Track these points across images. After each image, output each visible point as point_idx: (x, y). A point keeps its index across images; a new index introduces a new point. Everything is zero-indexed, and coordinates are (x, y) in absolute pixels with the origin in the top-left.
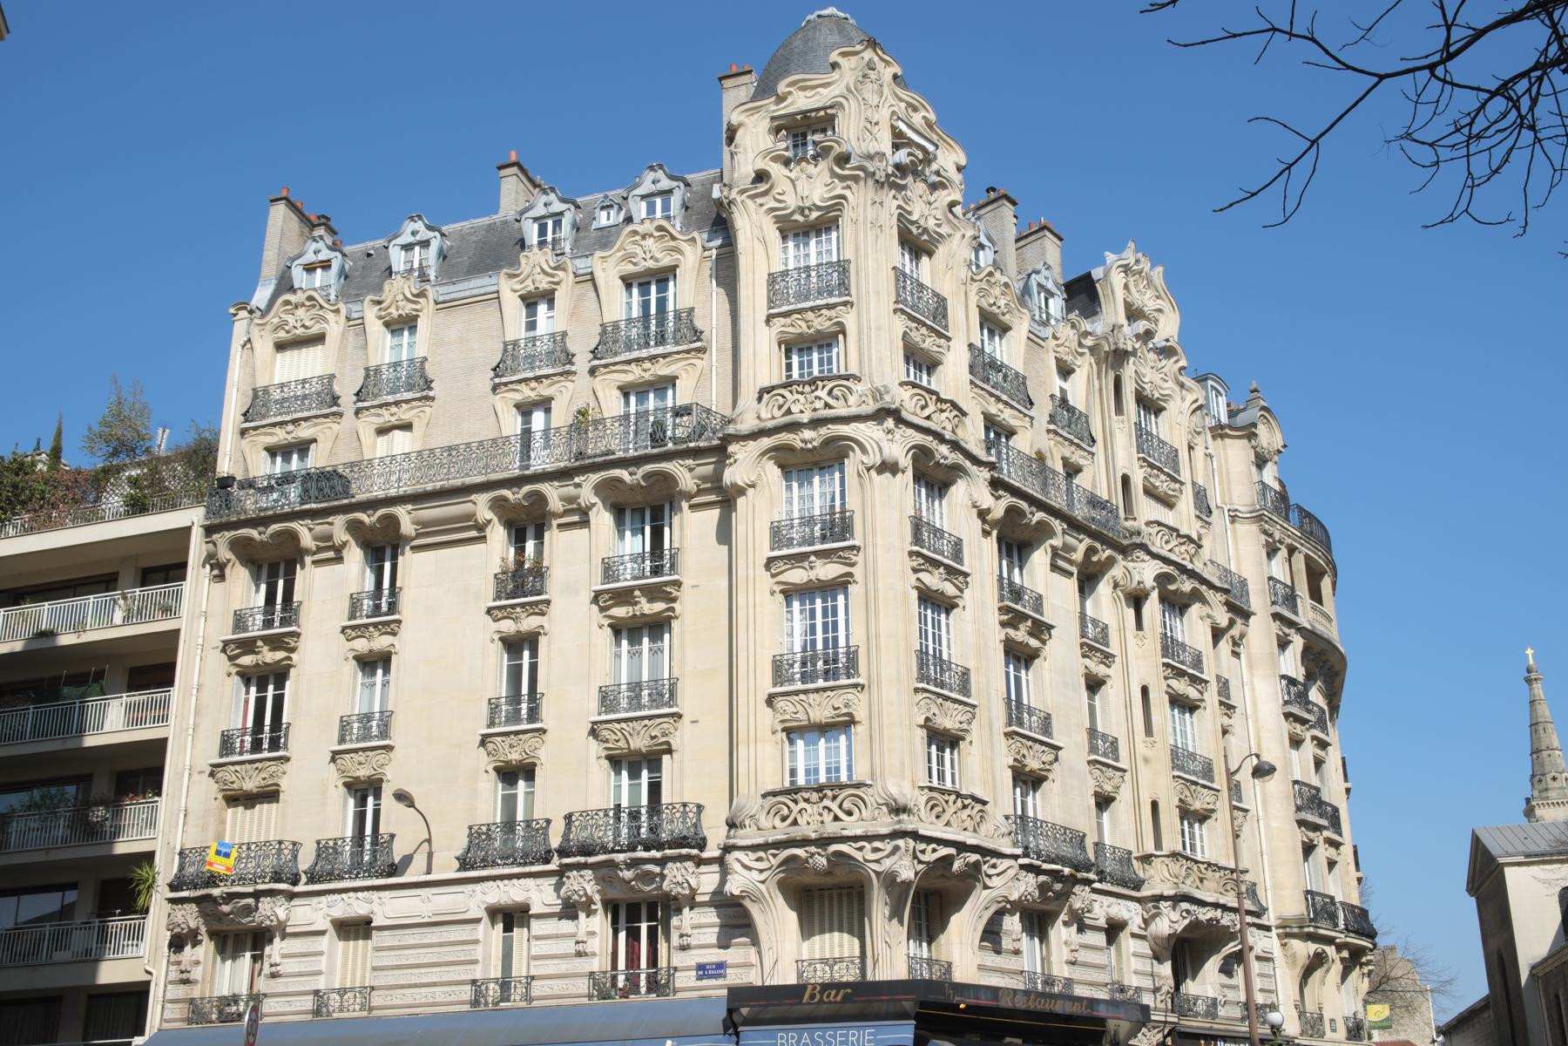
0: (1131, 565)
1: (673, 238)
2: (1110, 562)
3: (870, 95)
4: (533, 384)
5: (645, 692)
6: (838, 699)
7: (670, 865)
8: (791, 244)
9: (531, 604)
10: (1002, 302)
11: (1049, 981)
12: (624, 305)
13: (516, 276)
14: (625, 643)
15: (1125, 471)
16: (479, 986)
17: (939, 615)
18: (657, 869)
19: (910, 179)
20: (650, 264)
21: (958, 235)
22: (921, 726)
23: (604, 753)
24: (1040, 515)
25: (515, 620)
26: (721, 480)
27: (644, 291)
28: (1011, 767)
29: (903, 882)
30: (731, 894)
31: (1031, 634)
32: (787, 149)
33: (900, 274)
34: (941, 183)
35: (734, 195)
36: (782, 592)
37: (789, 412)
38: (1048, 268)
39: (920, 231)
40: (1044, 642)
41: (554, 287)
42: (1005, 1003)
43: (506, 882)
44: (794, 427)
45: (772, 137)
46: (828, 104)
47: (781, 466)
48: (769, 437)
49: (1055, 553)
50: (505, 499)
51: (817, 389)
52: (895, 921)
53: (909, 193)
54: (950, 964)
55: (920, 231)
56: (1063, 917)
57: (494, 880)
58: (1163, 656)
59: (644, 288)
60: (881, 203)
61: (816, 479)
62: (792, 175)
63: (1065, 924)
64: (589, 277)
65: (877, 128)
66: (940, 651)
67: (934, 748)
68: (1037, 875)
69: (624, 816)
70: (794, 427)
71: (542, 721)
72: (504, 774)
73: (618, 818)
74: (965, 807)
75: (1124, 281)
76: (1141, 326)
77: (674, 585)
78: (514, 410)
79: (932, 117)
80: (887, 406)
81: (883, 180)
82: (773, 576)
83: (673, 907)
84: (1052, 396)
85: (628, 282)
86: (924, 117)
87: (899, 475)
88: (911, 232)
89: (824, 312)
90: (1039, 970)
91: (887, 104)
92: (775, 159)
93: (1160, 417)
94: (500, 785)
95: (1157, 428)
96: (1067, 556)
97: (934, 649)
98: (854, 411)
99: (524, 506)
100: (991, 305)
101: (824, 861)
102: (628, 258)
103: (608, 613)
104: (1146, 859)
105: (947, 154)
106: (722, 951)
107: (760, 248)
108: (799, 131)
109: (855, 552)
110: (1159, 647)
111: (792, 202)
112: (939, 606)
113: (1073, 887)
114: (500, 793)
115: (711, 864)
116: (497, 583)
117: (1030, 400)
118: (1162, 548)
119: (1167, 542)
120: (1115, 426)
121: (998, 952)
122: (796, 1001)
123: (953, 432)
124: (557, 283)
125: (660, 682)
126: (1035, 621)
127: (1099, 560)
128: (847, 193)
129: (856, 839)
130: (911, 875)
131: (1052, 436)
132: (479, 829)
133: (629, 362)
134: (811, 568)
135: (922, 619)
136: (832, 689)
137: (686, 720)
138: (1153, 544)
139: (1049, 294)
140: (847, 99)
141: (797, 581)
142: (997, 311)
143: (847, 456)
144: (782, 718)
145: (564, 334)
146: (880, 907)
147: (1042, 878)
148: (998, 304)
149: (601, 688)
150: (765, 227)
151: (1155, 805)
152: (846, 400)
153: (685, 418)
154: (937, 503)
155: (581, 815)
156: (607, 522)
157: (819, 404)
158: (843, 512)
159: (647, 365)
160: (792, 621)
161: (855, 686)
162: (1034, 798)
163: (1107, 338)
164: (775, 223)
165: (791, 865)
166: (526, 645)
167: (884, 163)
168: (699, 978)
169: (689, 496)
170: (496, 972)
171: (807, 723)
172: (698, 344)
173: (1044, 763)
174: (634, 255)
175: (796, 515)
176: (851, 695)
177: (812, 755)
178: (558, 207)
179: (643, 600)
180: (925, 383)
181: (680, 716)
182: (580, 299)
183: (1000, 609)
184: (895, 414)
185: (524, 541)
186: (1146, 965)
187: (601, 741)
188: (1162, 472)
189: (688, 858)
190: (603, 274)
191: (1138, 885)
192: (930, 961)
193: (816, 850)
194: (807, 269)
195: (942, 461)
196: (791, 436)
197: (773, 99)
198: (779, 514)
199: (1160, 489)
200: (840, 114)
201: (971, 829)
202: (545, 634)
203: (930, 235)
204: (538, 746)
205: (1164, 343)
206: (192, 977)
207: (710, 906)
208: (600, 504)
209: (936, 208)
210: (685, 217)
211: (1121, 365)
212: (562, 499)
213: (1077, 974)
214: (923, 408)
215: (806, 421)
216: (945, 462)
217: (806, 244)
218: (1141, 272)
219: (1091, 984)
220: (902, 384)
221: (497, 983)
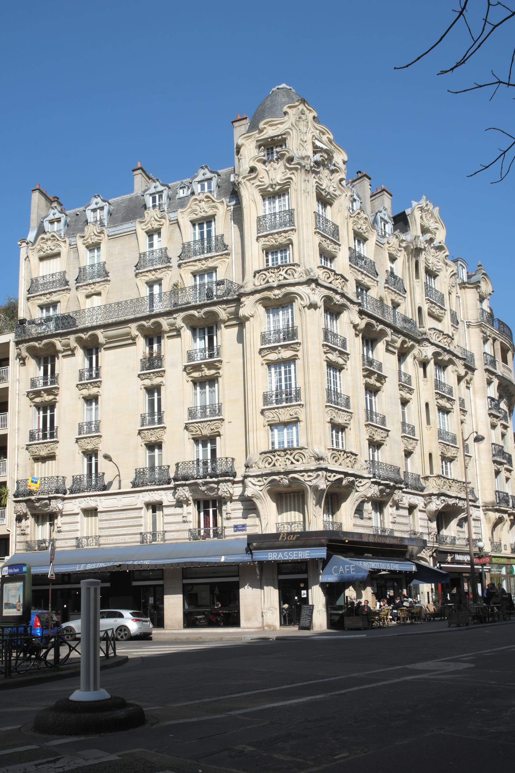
0: (422, 348)
1: (213, 202)
2: (413, 347)
3: (302, 127)
4: (153, 273)
5: (208, 410)
7: (221, 484)
9: (157, 372)
10: (364, 227)
11: (384, 530)
14: (198, 388)
15: (420, 305)
17: (336, 373)
18: (216, 486)
19: (321, 168)
20: (203, 214)
21: (344, 195)
22: (329, 422)
23: (192, 437)
24: (381, 327)
27: (201, 227)
29: (321, 490)
31: (377, 380)
32: (264, 156)
33: (317, 215)
34: (336, 170)
35: (240, 179)
36: (266, 364)
37: (268, 282)
38: (385, 210)
40: (382, 384)
42: (365, 539)
43: (152, 492)
44: (270, 289)
45: (257, 150)
47: (265, 307)
49: (387, 343)
50: (143, 326)
51: (280, 271)
52: (318, 506)
53: (321, 175)
54: (341, 524)
56: (390, 503)
58: (435, 389)
59: (201, 225)
60: (308, 181)
61: (281, 313)
62: (267, 169)
63: (391, 506)
64: (176, 221)
65: (306, 144)
66: (337, 389)
67: (334, 431)
68: (379, 486)
69: (201, 464)
70: (270, 289)
73: (198, 465)
74: (348, 457)
76: (428, 236)
78: (146, 285)
79: (331, 137)
80: (312, 278)
81: (309, 169)
82: (263, 357)
85: (193, 223)
86: (328, 138)
87: (318, 309)
88: (322, 194)
89: (283, 234)
90: (379, 526)
92: (259, 161)
93: (436, 279)
94: (148, 451)
97: (334, 388)
98: (297, 280)
100: (359, 229)
101: (287, 481)
102: (193, 212)
103: (190, 375)
104: (426, 478)
106: (244, 520)
107: (253, 204)
108: (270, 147)
111: (267, 182)
112: (336, 369)
117: (377, 273)
118: (436, 340)
119: (438, 337)
120: (415, 284)
121: (362, 518)
123: (342, 289)
126: (379, 374)
127: (407, 346)
128: (292, 176)
129: (301, 471)
130: (325, 487)
133: (195, 261)
134: (279, 353)
135: (329, 375)
136: (289, 406)
137: (226, 421)
139: (386, 222)
140: (292, 130)
141: (273, 359)
142: (362, 231)
143: (294, 302)
144: (268, 420)
145: (166, 249)
147: (381, 487)
148: (362, 228)
150: (255, 195)
152: (293, 276)
153: (222, 286)
154: (335, 322)
156: (188, 335)
157: (281, 278)
158: (293, 327)
159: (204, 262)
160: (271, 377)
161: (300, 405)
162: (378, 453)
163: (412, 243)
165: (273, 483)
166: (156, 391)
167: (310, 161)
168: (235, 531)
169: (224, 322)
170: (150, 529)
172: (226, 252)
174: (196, 210)
175: (272, 329)
176: (298, 409)
177: (281, 436)
178: (160, 188)
179: (206, 369)
180: (329, 267)
181: (223, 420)
182: (172, 232)
183: (363, 369)
184: (315, 281)
186: (425, 523)
189: (229, 481)
190: (182, 220)
194: (275, 214)
195: (337, 303)
196: (269, 293)
197: (257, 131)
198: (264, 329)
199: (435, 313)
200: (288, 138)
202: (164, 385)
203: (331, 196)
204: (163, 434)
205: (438, 244)
208: (185, 327)
209: (334, 182)
210: (218, 191)
213: (395, 527)
214: (328, 278)
215: (275, 286)
217: (274, 202)
218: (428, 210)
219: (401, 531)
220: (319, 267)
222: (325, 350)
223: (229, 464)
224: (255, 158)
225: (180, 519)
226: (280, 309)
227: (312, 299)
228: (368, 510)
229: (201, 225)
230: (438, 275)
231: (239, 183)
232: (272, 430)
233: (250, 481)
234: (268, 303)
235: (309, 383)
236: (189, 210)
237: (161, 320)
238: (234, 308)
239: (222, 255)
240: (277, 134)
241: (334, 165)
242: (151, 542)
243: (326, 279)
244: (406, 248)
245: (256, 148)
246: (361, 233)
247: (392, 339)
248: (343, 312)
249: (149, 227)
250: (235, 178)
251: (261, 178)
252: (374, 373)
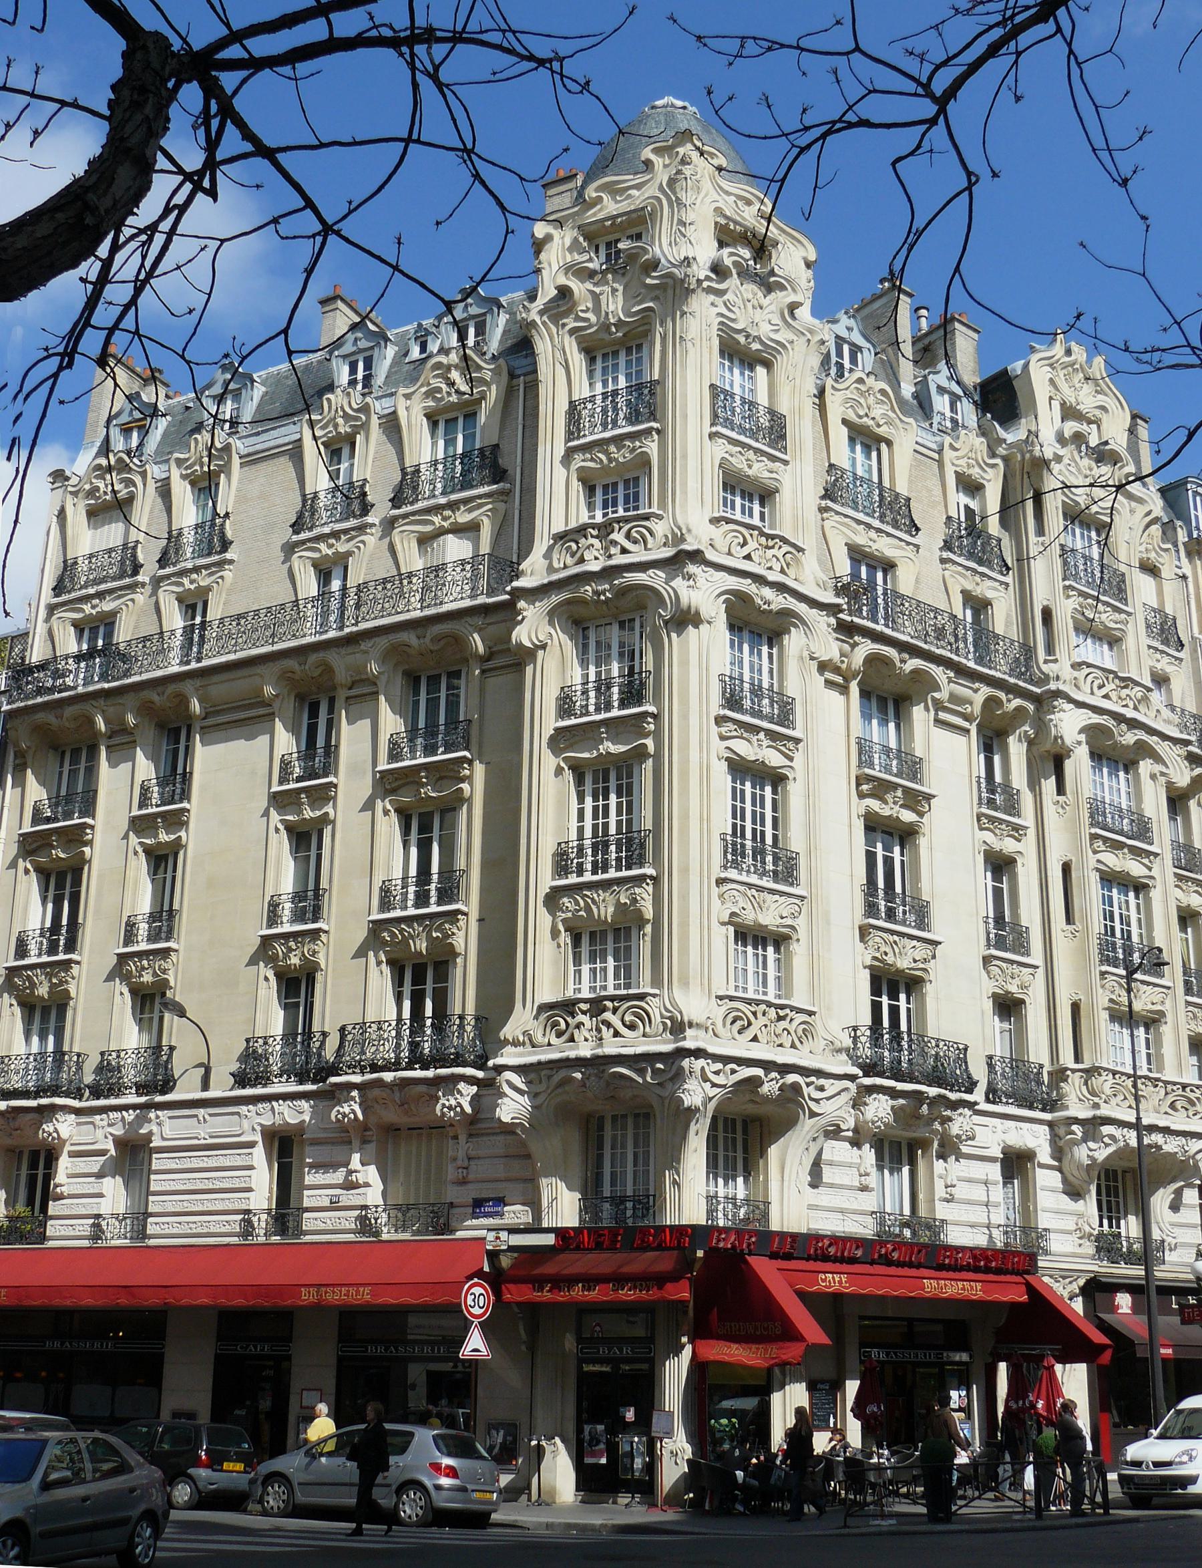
15: (1045, 603)
17: (762, 789)
24: (914, 663)
37: (582, 560)
51: (613, 531)
74: (780, 1018)
88: (739, 343)
91: (708, 200)
96: (959, 709)
119: (1100, 687)
126: (906, 790)
174: (439, 390)
180: (756, 521)
194: (615, 393)
220: (715, 521)
221: (399, 1210)
224: (569, 269)
233: (509, 1083)
234: (582, 611)
236: (424, 389)
249: (330, 432)
251: (582, 311)
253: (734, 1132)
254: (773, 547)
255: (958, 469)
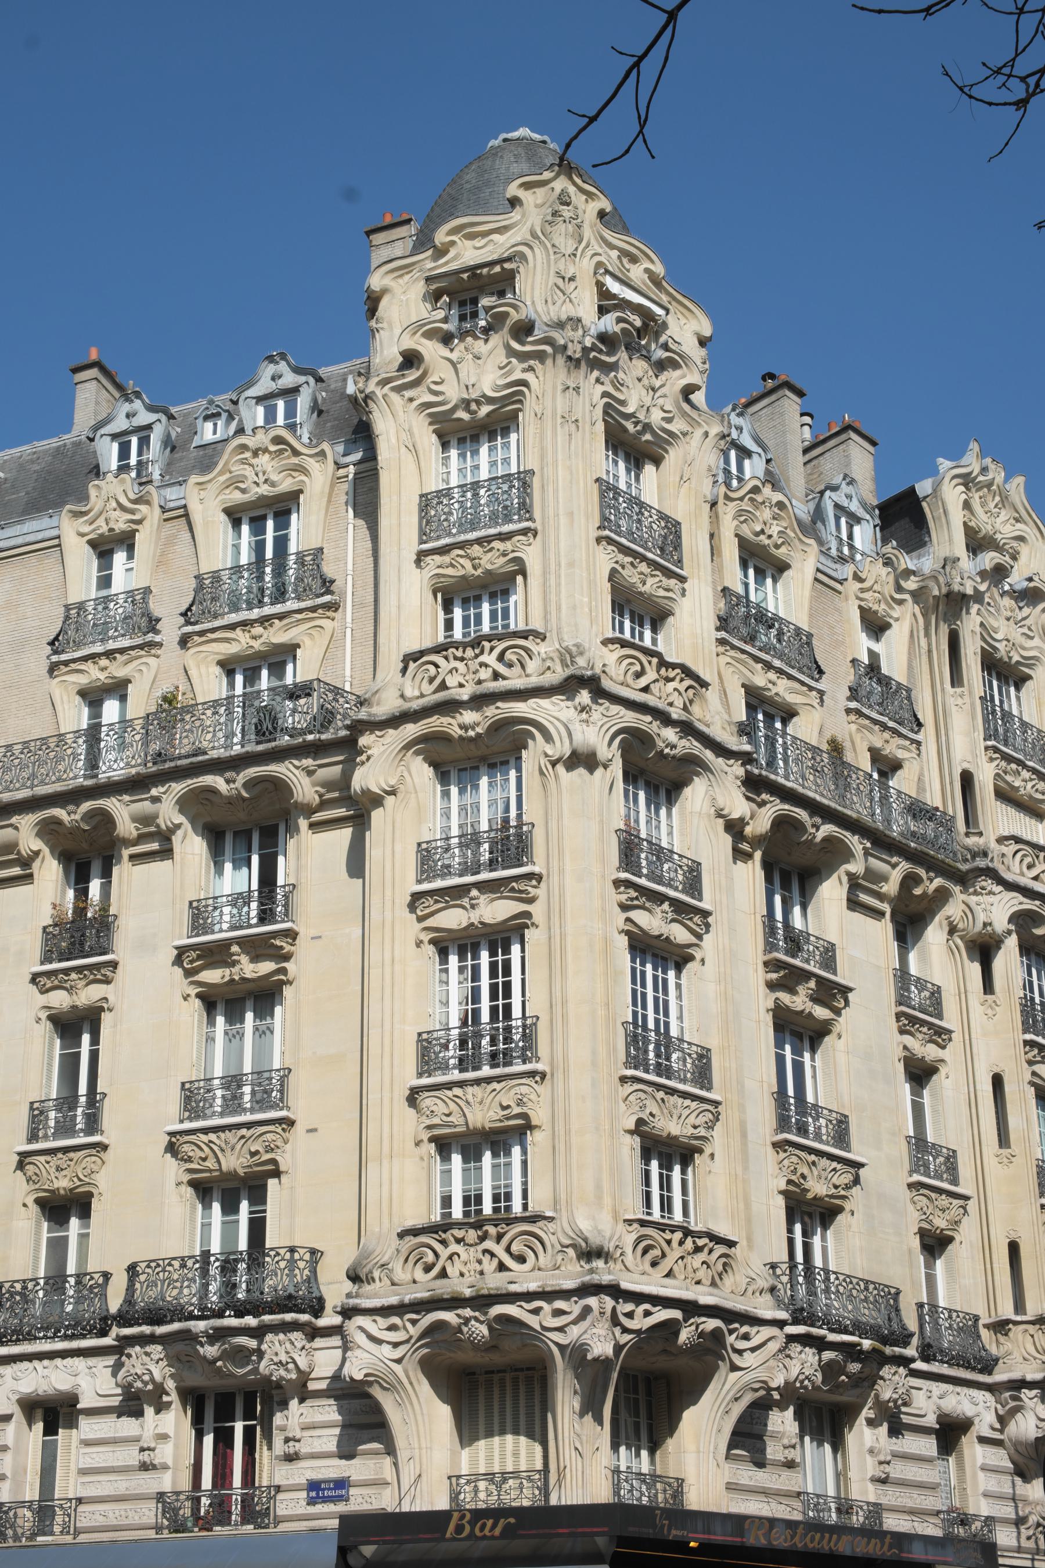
0: (973, 899)
1: (296, 453)
2: (942, 896)
3: (562, 239)
4: (104, 662)
5: (247, 1089)
6: (508, 1094)
7: (269, 1337)
8: (454, 453)
9: (90, 967)
10: (774, 530)
11: (845, 1508)
12: (230, 548)
13: (83, 514)
14: (220, 1020)
15: (966, 766)
16: (6, 1512)
17: (665, 972)
18: (253, 1343)
19: (622, 355)
20: (264, 490)
21: (698, 433)
22: (631, 1132)
23: (187, 1177)
24: (827, 829)
25: (69, 990)
26: (349, 787)
27: (258, 529)
28: (784, 1193)
29: (596, 1360)
30: (351, 1378)
31: (815, 1000)
32: (445, 320)
33: (607, 489)
34: (669, 359)
35: (371, 387)
36: (432, 942)
37: (443, 686)
38: (852, 482)
39: (639, 428)
40: (837, 1012)
41: (135, 527)
42: (755, 1539)
43: (46, 1362)
44: (449, 707)
45: (429, 306)
46: (505, 255)
47: (435, 764)
48: (415, 722)
49: (854, 884)
50: (58, 822)
51: (482, 652)
52: (588, 1418)
53: (621, 375)
54: (681, 1481)
55: (639, 428)
56: (867, 1412)
57: (30, 1361)
58: (1025, 1032)
59: (258, 524)
60: (577, 389)
61: (484, 782)
62: (454, 356)
63: (870, 1423)
64: (181, 512)
65: (573, 285)
66: (667, 1025)
67: (654, 1164)
68: (820, 1351)
69: (214, 1270)
70: (449, 707)
71: (102, 1133)
72: (51, 1208)
73: (204, 1272)
74: (698, 1249)
75: (964, 496)
76: (988, 559)
77: (286, 936)
78: (78, 698)
79: (659, 269)
80: (578, 673)
81: (578, 355)
82: (420, 919)
83: (276, 1399)
84: (854, 661)
85: (234, 516)
86: (647, 271)
87: (599, 772)
88: (625, 430)
89: (496, 544)
90: (831, 1492)
92: (429, 335)
93: (1024, 690)
94: (46, 1224)
95: (1020, 705)
96: (874, 887)
97: (657, 1021)
98: (534, 681)
99: (85, 831)
100: (757, 534)
101: (484, 1330)
102: (235, 482)
103: (196, 978)
104: (1001, 1327)
105: (683, 321)
106: (343, 1462)
107: (408, 459)
108: (467, 296)
109: (534, 882)
110: (944, 1003)
111: (453, 393)
112: (665, 959)
113: (880, 1369)
114: (45, 1235)
115: (330, 1335)
116: (47, 940)
117: (818, 667)
118: (1022, 874)
119: (1030, 867)
120: (951, 701)
121: (760, 1463)
122: (437, 1535)
123: (685, 708)
124: (139, 522)
125: (266, 1075)
126: (820, 980)
127: (925, 894)
128: (529, 377)
129: (529, 1296)
130: (608, 1350)
131: (853, 717)
132: (12, 1286)
133: (232, 627)
134: (473, 907)
135: (637, 978)
136: (499, 1079)
137: (300, 1128)
138: (1008, 869)
139: (854, 519)
140: (531, 247)
141: (454, 926)
142: (767, 542)
143: (525, 747)
144: (428, 1122)
145: (147, 591)
146: (567, 1399)
147: (828, 1355)
148: (768, 532)
149: (183, 1084)
150: (416, 430)
151: (1014, 1248)
152: (523, 667)
153: (302, 701)
154: (663, 812)
155: (148, 1266)
156: (197, 851)
157: (485, 674)
158: (519, 826)
159: (258, 630)
160: (447, 983)
161: (532, 1074)
162: (824, 1239)
163: (935, 578)
164: (431, 424)
165: (438, 1336)
166: (86, 1026)
167: (580, 332)
168: (311, 1502)
169: (309, 811)
170: (31, 1492)
171: (463, 1129)
172: (327, 598)
173: (836, 1187)
174: (242, 479)
175: (455, 831)
176: (525, 1088)
177: (472, 1175)
178: (144, 417)
179: (244, 959)
180: (647, 642)
181: (291, 1123)
182: (170, 542)
183: (766, 964)
184: (593, 684)
185: (87, 881)
186: (1004, 1485)
187: (182, 1159)
188: (1025, 766)
189: (295, 1326)
190: (200, 507)
191: (988, 1365)
192: (655, 1477)
193: (472, 1314)
194: (476, 486)
195: (667, 751)
196: (446, 720)
197: (430, 252)
198: (431, 831)
199: (1022, 792)
200: (521, 270)
201: (707, 1281)
202: (110, 1010)
203: (654, 433)
204: (95, 1168)
205: (1025, 584)
206: (158, 1457)
207: (329, 1397)
208: (187, 825)
209: (665, 396)
210: (317, 425)
211: (958, 616)
212: (135, 819)
213: (889, 1496)
214: (638, 675)
215: (465, 698)
216: (673, 752)
217: (475, 453)
218: (989, 485)
219: (912, 1512)
220: (606, 642)
222: (623, 898)
223: (302, 1271)
225: (131, 1456)
226: (483, 769)
227: (578, 738)
228: (783, 1434)
229: (258, 524)
230: (1029, 677)
231: (367, 398)
232: (446, 1158)
233: (360, 1328)
234: (444, 752)
235: (564, 1003)
237: (115, 806)
238: (341, 766)
239: (313, 609)
240: (490, 259)
241: (666, 347)
242: (33, 1536)
243: (630, 679)
244: (917, 595)
245: (425, 299)
246: (764, 547)
247: (868, 870)
248: (691, 780)
250: (355, 383)
252: (806, 975)
253: (636, 1392)
254: (672, 680)
255: (862, 604)
